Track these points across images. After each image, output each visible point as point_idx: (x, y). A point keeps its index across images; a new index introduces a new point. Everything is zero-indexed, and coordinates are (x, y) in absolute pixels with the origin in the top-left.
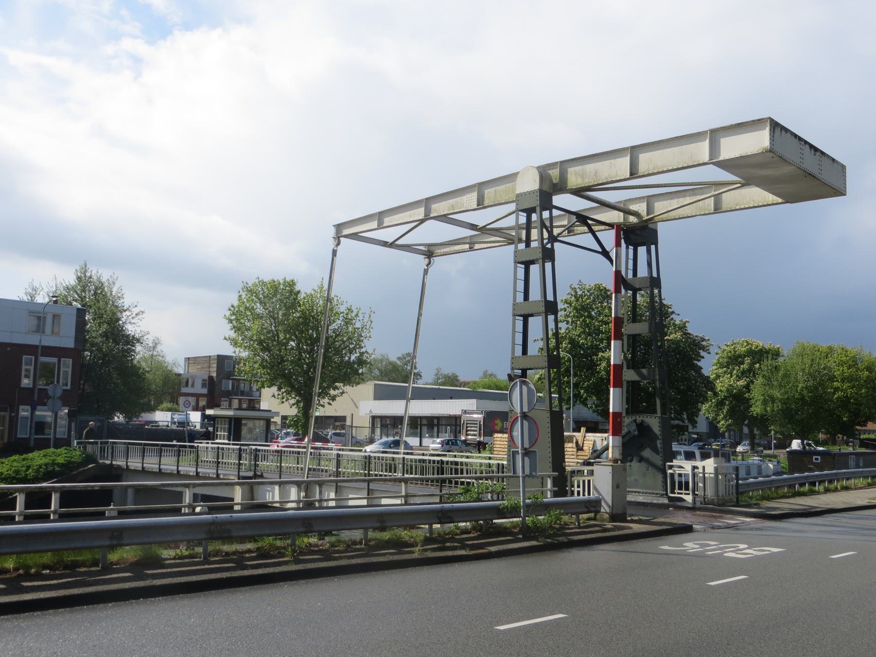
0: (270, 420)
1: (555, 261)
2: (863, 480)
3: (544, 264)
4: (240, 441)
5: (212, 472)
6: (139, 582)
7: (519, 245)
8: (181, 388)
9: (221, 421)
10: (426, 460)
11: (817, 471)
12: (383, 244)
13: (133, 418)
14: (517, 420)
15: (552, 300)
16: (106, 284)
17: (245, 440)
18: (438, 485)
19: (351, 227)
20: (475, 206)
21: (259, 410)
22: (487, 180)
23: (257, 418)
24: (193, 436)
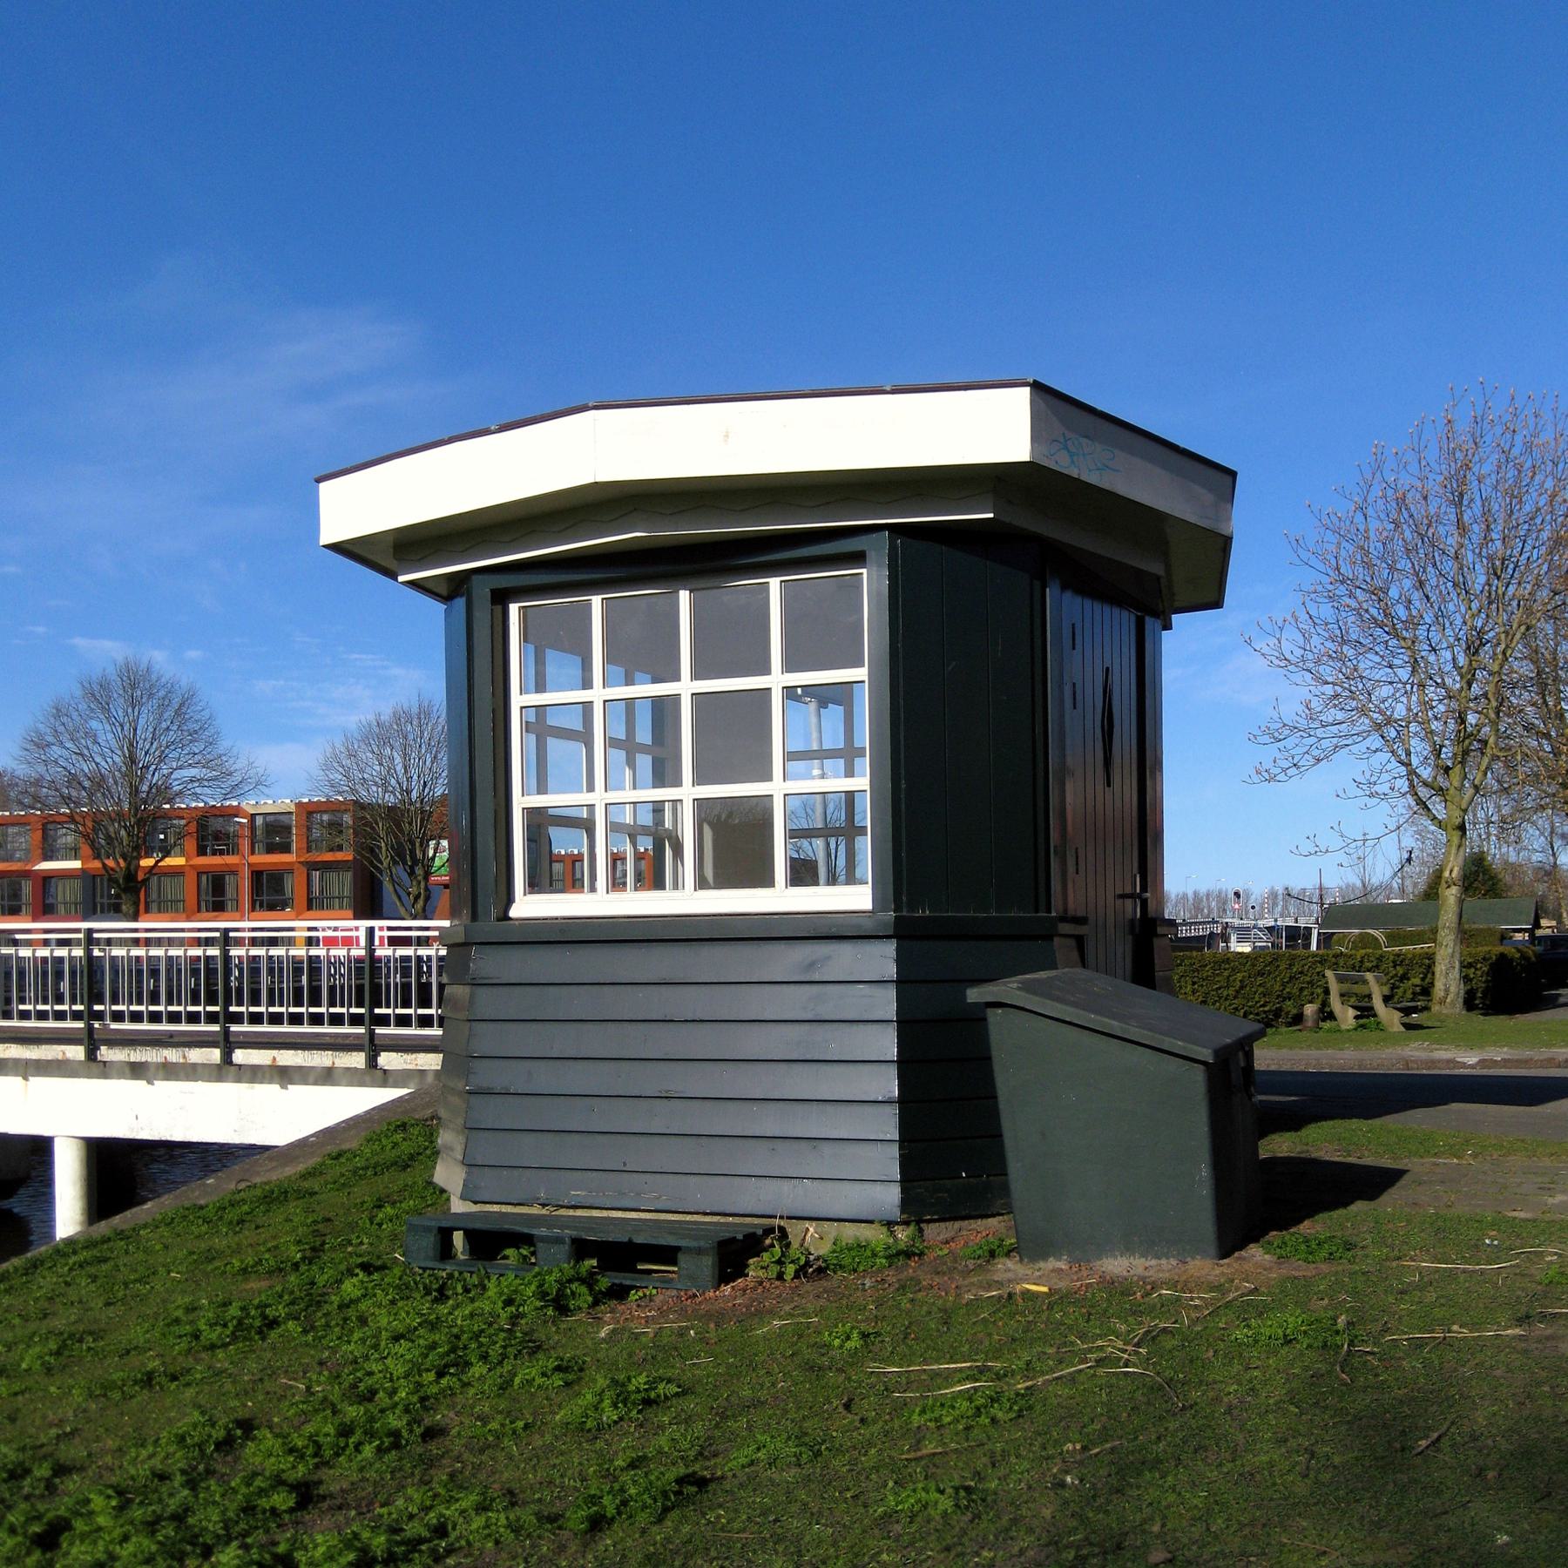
0: (1242, 1068)
1: (630, 1244)
2: (13, 1516)
3: (627, 736)
4: (865, 748)
5: (1344, 544)
6: (1050, 536)
7: (649, 758)
8: (1138, 610)
9: (1357, 892)
10: (244, 938)
11: (1129, 1249)
12: (127, 1070)
13: (666, 830)
14: (429, 585)
15: (580, 728)
16: (41, 769)
17: (526, 737)
18: (839, 695)
19: (115, 1138)
20: (990, 1012)
21: (510, 919)
22: (204, 1141)
23: (1148, 702)
24: (91, 1333)
